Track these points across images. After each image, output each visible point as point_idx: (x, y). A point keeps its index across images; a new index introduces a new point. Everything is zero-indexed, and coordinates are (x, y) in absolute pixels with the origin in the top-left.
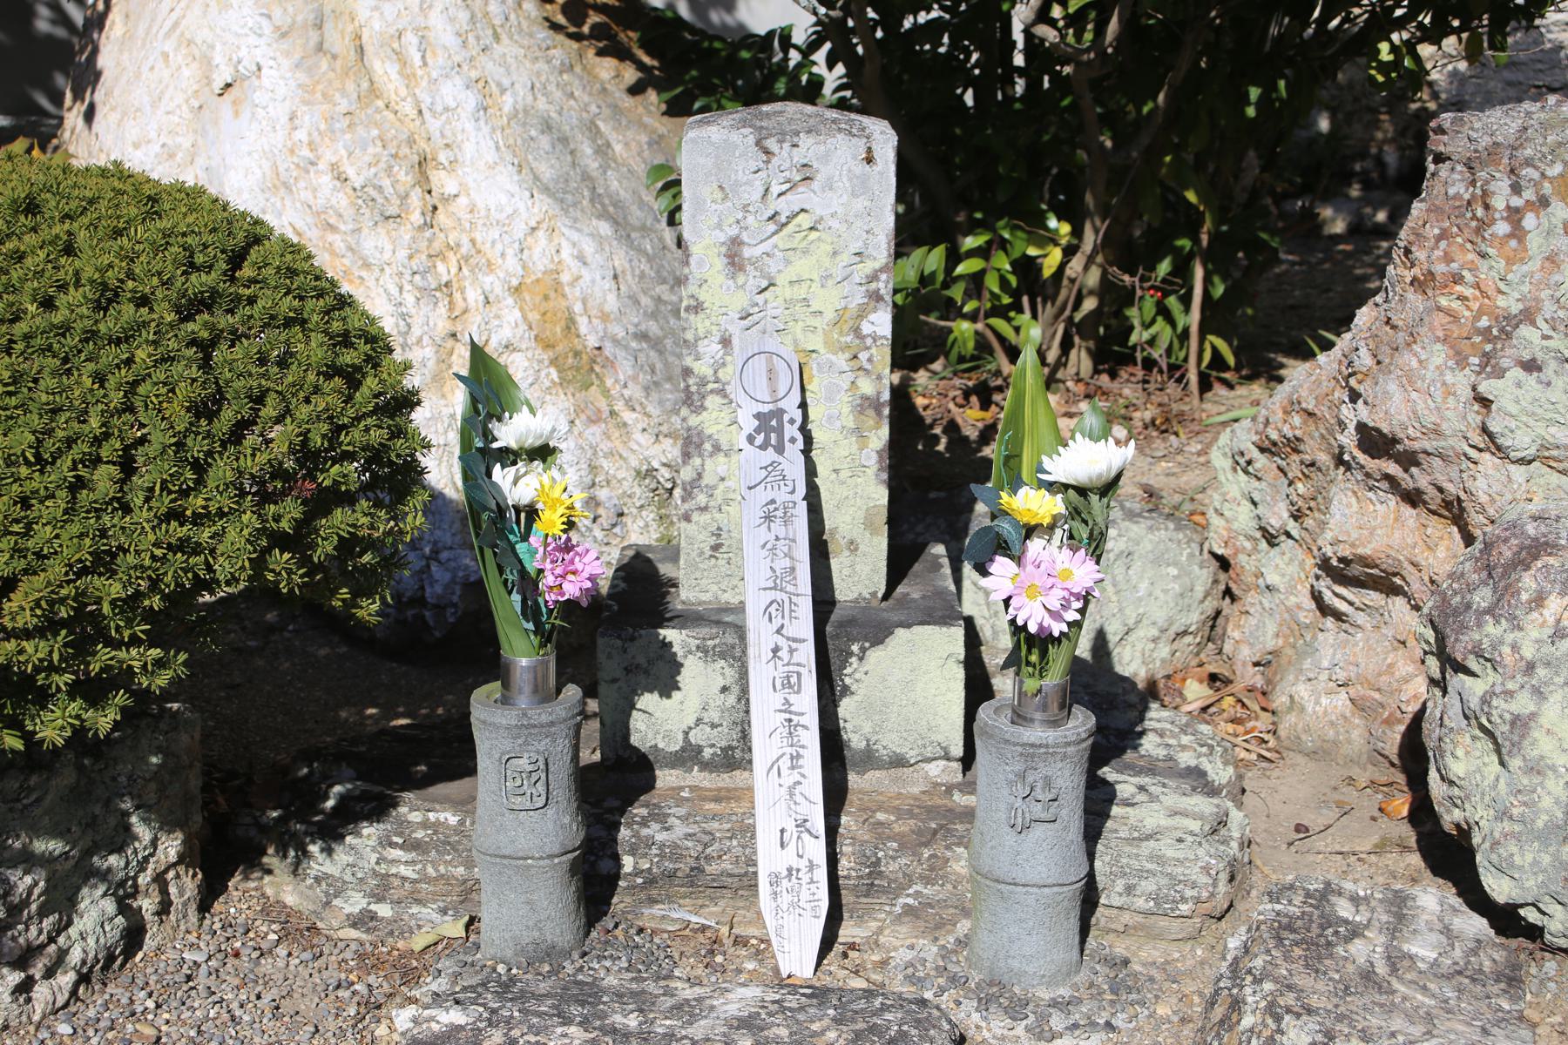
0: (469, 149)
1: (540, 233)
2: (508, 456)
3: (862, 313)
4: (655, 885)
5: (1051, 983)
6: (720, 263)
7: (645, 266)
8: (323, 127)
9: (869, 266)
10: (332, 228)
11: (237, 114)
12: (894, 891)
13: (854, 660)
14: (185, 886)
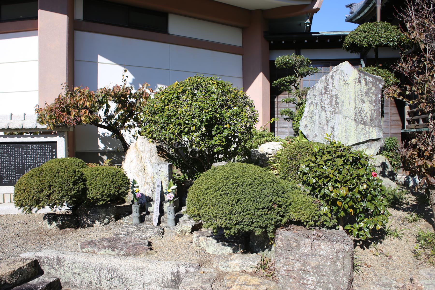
2: (135, 187)
4: (147, 221)
14: (114, 219)
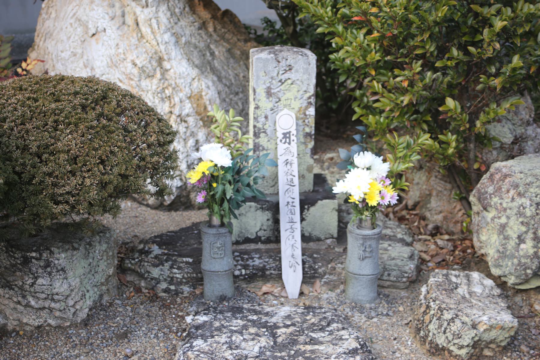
0: (173, 54)
1: (196, 80)
3: (307, 108)
5: (370, 303)
6: (264, 95)
7: (227, 89)
8: (128, 48)
9: (308, 95)
10: (132, 80)
11: (97, 43)
12: (322, 276)
13: (306, 210)
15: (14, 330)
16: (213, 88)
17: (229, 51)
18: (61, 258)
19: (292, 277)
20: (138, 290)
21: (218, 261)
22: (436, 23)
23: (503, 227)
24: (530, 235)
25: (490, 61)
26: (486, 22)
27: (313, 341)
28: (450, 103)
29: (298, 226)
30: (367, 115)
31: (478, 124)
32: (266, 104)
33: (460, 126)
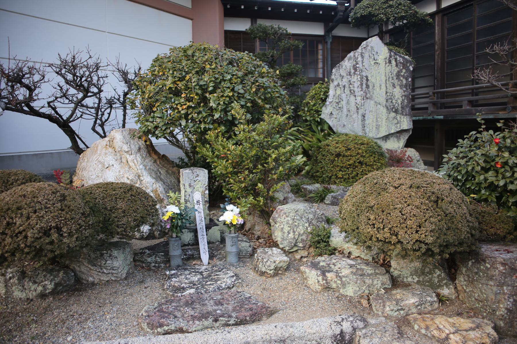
0: (144, 173)
3: (205, 191)
12: (216, 256)
15: (98, 283)
16: (161, 187)
17: (167, 171)
18: (115, 253)
19: (205, 256)
20: (143, 267)
21: (175, 251)
22: (252, 156)
23: (282, 229)
24: (292, 231)
25: (272, 169)
26: (269, 156)
27: (217, 275)
28: (260, 185)
29: (205, 236)
30: (228, 193)
31: (270, 193)
32: (189, 190)
33: (264, 194)
